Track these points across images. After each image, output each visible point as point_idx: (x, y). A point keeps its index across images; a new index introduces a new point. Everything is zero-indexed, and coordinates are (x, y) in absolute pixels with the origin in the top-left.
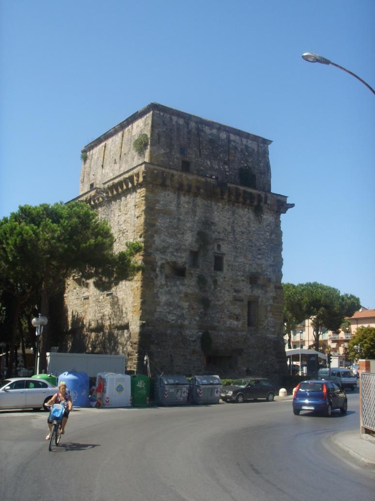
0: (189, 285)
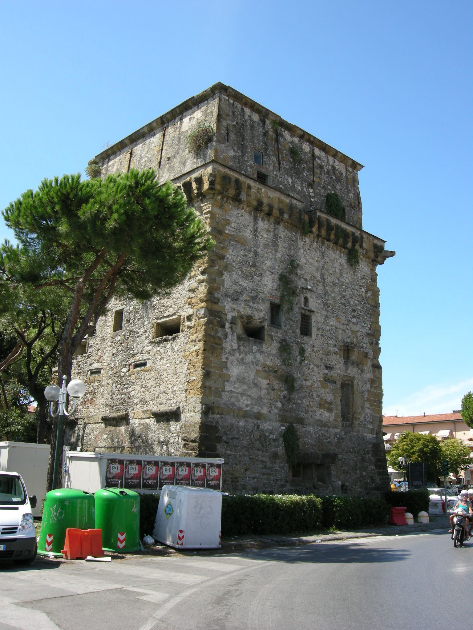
0: (267, 354)
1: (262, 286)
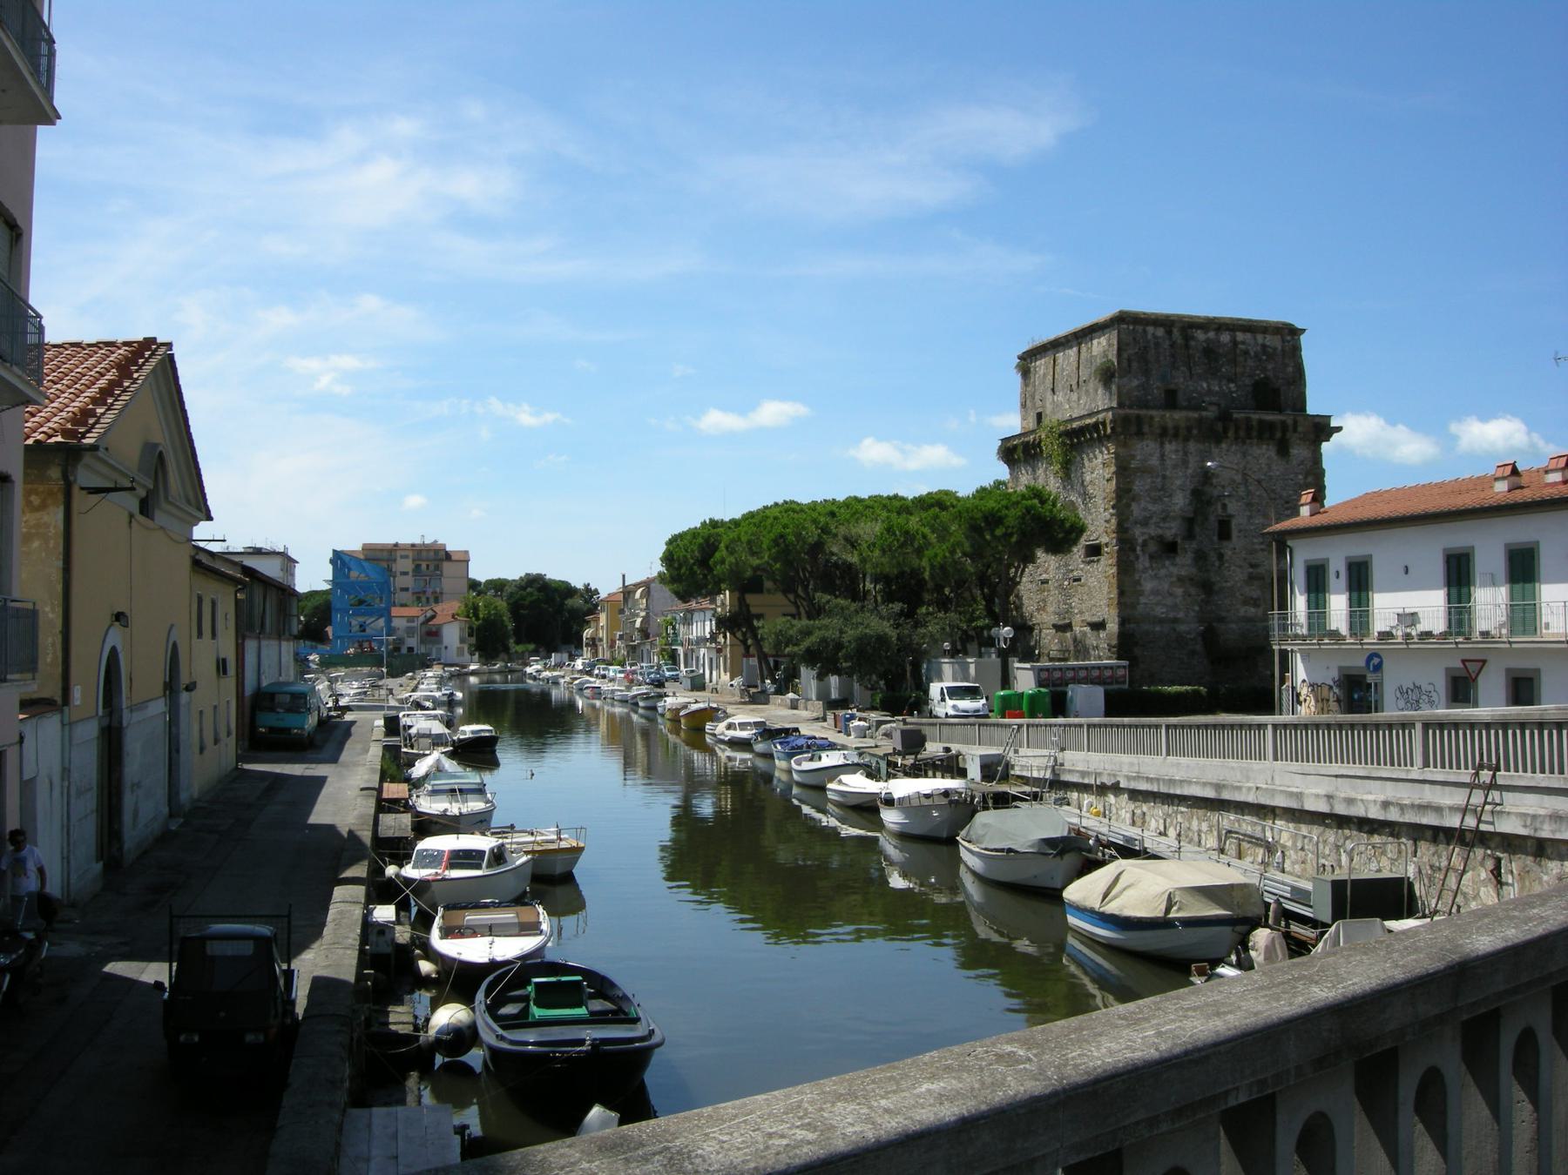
0: (1184, 564)
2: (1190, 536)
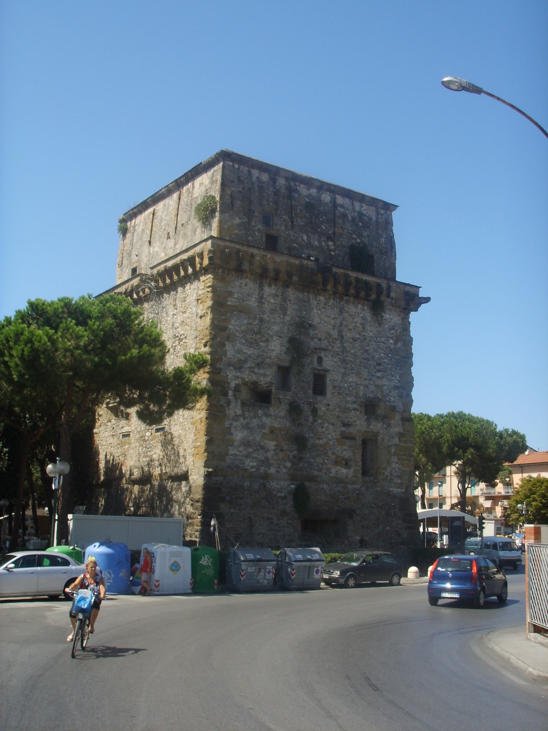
0: (276, 416)
1: (268, 352)
2: (284, 385)
